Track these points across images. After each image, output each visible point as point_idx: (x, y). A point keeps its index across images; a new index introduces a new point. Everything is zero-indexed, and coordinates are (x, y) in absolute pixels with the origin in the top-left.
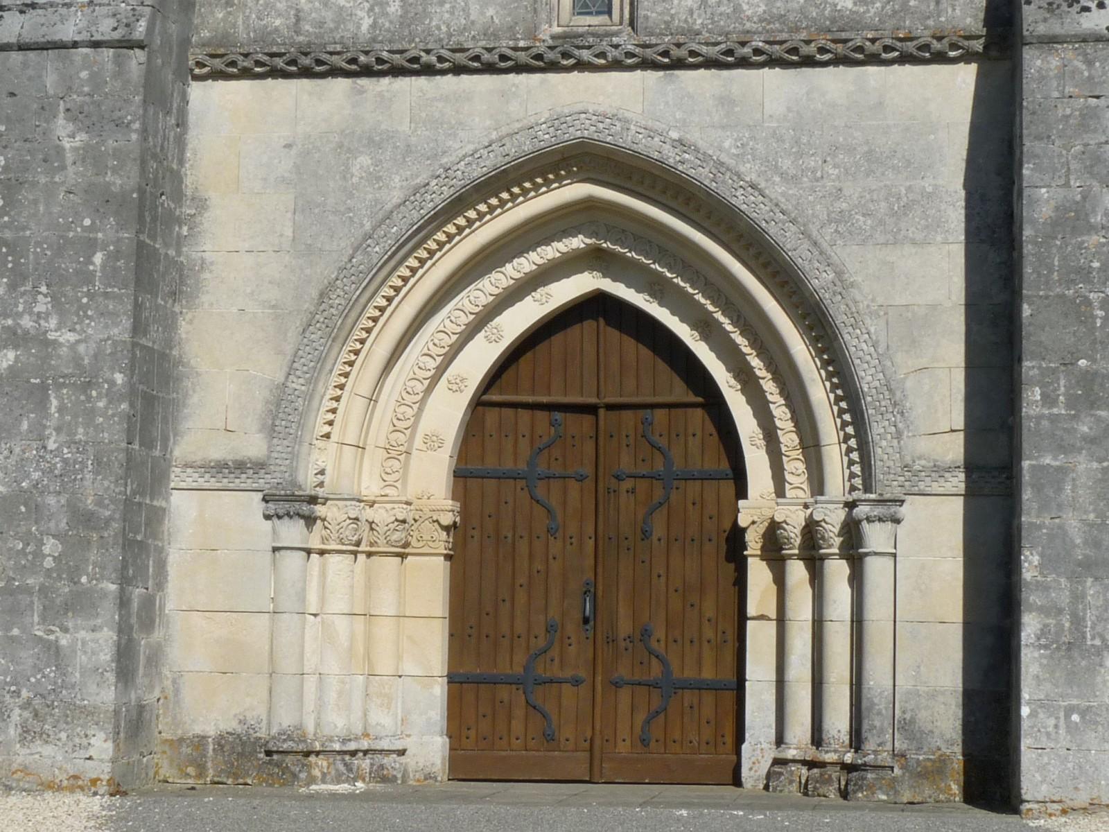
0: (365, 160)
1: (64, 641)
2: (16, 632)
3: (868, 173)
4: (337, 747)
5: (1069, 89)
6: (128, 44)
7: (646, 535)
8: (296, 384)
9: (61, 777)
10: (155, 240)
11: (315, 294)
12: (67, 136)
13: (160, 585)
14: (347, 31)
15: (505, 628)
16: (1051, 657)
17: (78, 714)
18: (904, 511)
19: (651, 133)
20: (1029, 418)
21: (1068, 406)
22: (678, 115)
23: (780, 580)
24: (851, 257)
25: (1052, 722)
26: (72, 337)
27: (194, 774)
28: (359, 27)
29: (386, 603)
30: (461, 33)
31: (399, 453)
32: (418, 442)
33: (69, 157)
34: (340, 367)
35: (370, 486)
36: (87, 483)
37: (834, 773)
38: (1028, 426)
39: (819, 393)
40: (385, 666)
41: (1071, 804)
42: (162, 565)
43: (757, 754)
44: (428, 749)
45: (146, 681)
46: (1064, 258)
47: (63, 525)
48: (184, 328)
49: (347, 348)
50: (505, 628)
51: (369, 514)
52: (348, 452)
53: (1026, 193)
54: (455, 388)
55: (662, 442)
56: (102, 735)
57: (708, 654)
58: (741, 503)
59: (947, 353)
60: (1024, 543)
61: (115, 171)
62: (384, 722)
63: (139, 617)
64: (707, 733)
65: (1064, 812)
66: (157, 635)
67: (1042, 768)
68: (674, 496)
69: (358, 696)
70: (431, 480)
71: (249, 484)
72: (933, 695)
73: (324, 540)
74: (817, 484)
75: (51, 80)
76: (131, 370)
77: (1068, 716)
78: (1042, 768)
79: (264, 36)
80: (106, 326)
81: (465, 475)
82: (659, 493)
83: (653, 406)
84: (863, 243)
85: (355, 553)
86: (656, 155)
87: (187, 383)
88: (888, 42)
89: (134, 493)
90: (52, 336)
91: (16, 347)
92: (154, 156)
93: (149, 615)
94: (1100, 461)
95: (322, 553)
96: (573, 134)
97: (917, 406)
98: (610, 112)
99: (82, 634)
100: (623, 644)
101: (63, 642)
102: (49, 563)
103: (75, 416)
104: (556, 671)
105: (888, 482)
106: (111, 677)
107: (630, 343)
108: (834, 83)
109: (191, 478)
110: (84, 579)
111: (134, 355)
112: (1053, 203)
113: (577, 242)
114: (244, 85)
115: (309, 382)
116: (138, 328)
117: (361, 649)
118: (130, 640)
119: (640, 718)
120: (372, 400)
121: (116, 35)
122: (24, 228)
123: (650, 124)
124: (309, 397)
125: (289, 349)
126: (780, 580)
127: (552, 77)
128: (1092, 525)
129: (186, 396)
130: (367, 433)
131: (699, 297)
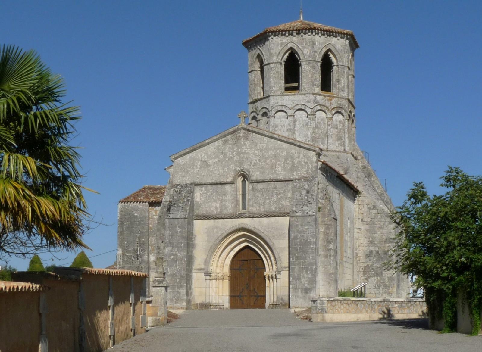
1: (180, 291)
6: (185, 218)
7: (254, 277)
8: (208, 259)
12: (179, 230)
13: (192, 284)
14: (213, 214)
17: (182, 300)
18: (281, 273)
19: (250, 226)
24: (274, 241)
27: (198, 195)
29: (220, 286)
32: (225, 265)
39: (272, 258)
40: (221, 294)
42: (192, 282)
43: (267, 304)
44: (227, 305)
48: (194, 252)
51: (218, 275)
54: (229, 258)
66: (191, 291)
69: (217, 298)
70: (226, 270)
72: (285, 295)
75: (176, 223)
81: (232, 269)
96: (241, 226)
97: (283, 260)
108: (272, 219)
109: (195, 271)
113: (244, 239)
114: (201, 220)
116: (188, 253)
117: (217, 292)
127: (238, 219)
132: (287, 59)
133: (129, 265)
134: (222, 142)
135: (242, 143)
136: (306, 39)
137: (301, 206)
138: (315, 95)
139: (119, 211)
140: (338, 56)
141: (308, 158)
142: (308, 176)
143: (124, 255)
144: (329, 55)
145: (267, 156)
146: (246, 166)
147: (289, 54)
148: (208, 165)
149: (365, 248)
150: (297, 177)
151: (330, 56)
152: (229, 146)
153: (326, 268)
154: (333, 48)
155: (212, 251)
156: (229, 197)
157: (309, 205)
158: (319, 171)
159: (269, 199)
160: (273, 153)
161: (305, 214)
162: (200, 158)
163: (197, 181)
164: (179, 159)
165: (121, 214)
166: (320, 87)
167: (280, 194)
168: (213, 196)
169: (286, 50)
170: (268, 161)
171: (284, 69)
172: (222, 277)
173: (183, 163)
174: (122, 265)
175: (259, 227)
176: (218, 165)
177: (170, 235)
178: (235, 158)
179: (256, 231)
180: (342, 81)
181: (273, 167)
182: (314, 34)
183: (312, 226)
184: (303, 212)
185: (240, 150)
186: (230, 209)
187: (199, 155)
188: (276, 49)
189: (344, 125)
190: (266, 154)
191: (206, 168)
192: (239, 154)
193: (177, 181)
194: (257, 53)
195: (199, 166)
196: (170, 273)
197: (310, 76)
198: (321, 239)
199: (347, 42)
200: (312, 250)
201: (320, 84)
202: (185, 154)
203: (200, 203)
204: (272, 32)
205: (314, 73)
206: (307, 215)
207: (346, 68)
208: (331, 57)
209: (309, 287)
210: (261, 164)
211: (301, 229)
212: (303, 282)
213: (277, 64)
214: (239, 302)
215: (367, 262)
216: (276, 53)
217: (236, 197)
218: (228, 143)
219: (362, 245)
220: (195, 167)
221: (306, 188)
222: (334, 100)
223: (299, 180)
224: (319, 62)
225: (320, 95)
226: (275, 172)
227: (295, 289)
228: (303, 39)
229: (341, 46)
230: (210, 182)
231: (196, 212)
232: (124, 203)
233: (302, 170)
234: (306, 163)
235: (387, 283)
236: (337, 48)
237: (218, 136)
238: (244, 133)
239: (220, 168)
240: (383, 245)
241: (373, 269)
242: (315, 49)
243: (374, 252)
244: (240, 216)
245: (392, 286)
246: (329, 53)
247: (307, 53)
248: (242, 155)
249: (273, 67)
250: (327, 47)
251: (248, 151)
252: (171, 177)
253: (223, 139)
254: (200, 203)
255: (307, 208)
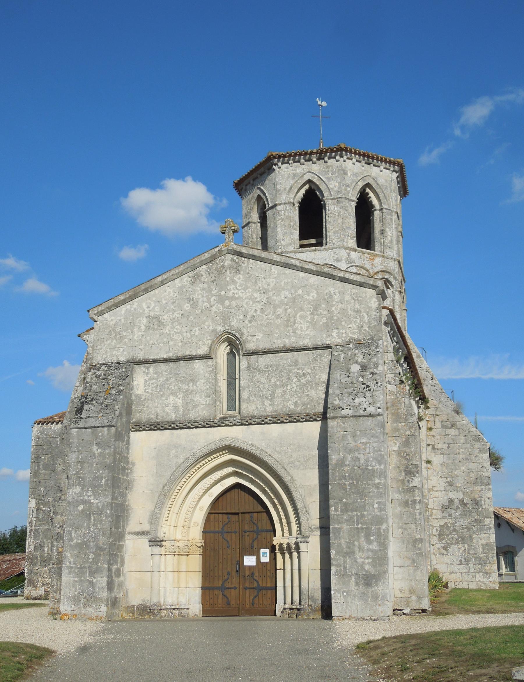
0: (174, 451)
2: (82, 578)
3: (299, 451)
4: (169, 607)
5: (339, 430)
9: (93, 617)
10: (119, 475)
11: (162, 487)
13: (122, 565)
14: (168, 419)
15: (216, 574)
16: (339, 578)
18: (309, 540)
19: (244, 442)
20: (331, 515)
21: (341, 512)
22: (251, 437)
23: (284, 558)
25: (339, 595)
26: (97, 501)
27: (141, 381)
28: (172, 417)
29: (183, 568)
30: (197, 418)
31: (187, 527)
32: (192, 524)
33: (97, 455)
34: (169, 506)
35: (179, 537)
36: (100, 539)
37: (295, 611)
38: (331, 517)
41: (344, 617)
43: (279, 607)
44: (195, 607)
45: (118, 591)
46: (339, 473)
47: (94, 550)
49: (171, 501)
50: (216, 574)
52: (172, 528)
53: (329, 457)
54: (201, 509)
55: (256, 522)
56: (103, 605)
57: (269, 580)
58: (274, 538)
59: (316, 498)
60: (331, 548)
61: (108, 458)
62: (183, 601)
63: (115, 573)
64: (269, 602)
65: (343, 619)
66: (121, 578)
67: (337, 608)
68: (259, 537)
70: (196, 535)
71: (145, 537)
73: (166, 552)
74: (290, 534)
76: (111, 510)
77: (343, 593)
78: (337, 608)
79: (149, 419)
80: (105, 498)
81: (207, 531)
82: (255, 536)
83: (253, 512)
84: (298, 469)
85: (174, 555)
86: (245, 448)
87: (130, 511)
88: (302, 417)
89: (113, 541)
90: (92, 501)
91: (83, 504)
92: (118, 454)
93: (118, 573)
94: (349, 526)
95: (165, 555)
96: (225, 443)
98: (234, 437)
99: (99, 578)
100: (247, 578)
101: (94, 581)
102: (91, 560)
103: (98, 522)
104: (230, 585)
105: (305, 532)
106: (106, 590)
107: (247, 495)
108: (290, 427)
110: (99, 564)
111: (112, 506)
112: (336, 459)
113: (230, 469)
115: (160, 510)
118: (112, 580)
119: (252, 598)
120: (178, 514)
121: (108, 424)
122: (86, 474)
123: (244, 440)
124: (160, 514)
125: (155, 502)
126: (284, 558)
128: (348, 543)
129: (130, 514)
130: (178, 520)
131: (261, 484)
132: (302, 200)
133: (47, 527)
134: (189, 279)
135: (228, 279)
136: (332, 166)
137: (351, 397)
138: (348, 251)
139: (33, 438)
140: (381, 195)
141: (360, 303)
142: (361, 337)
143: (38, 509)
144: (368, 194)
145: (277, 302)
146: (235, 323)
147: (307, 191)
148: (161, 324)
149: (440, 494)
150: (340, 341)
151: (370, 195)
152: (201, 285)
153: (405, 529)
154: (374, 182)
155: (164, 494)
156: (201, 384)
157: (367, 394)
158: (384, 326)
159: (282, 386)
160: (290, 296)
161: (362, 412)
162: (147, 310)
163: (141, 356)
164: (106, 316)
165: (37, 445)
166: (355, 239)
167: (304, 375)
168: (171, 384)
169: (302, 184)
170: (280, 311)
171: (298, 214)
172: (186, 550)
173: (113, 322)
174: (35, 526)
175: (262, 445)
176: (180, 324)
177: (78, 462)
178: (214, 308)
179: (257, 453)
180: (389, 233)
181: (290, 322)
182: (345, 158)
183: (377, 437)
184: (356, 407)
185: (223, 293)
186: (203, 409)
187: (145, 306)
188: (286, 184)
189: (393, 300)
190: (275, 298)
191: (157, 330)
192: (221, 300)
193: (99, 358)
194: (256, 195)
195: (143, 327)
196: (75, 541)
197: (340, 221)
198: (393, 466)
199: (395, 175)
200: (378, 488)
201: (355, 235)
202: (117, 306)
203: (143, 398)
204: (279, 157)
205: (347, 217)
206: (365, 413)
207: (394, 213)
208: (370, 197)
209: (372, 571)
210: (265, 317)
211: (354, 444)
212: (360, 561)
213: (287, 206)
214: (220, 601)
215: (444, 518)
216: (285, 189)
217: (216, 385)
218: (200, 280)
219: (435, 489)
220: (136, 329)
221: (359, 360)
222: (378, 261)
223: (343, 346)
224: (352, 201)
225: (355, 251)
226: (294, 332)
227: (343, 575)
228: (328, 167)
229: (386, 181)
230: (165, 356)
231: (136, 417)
232: (43, 424)
233: (351, 326)
234: (358, 312)
235: (481, 555)
236: (380, 184)
237: (182, 268)
238: (233, 260)
239: (184, 330)
240: (471, 489)
241: (455, 530)
242: (347, 182)
243: (457, 502)
244: (222, 423)
245: (491, 559)
246: (368, 190)
247: (335, 186)
248: (227, 303)
249: (281, 211)
250: (364, 181)
251: (240, 293)
252: (90, 349)
253: (191, 274)
254: (143, 398)
255: (364, 400)
